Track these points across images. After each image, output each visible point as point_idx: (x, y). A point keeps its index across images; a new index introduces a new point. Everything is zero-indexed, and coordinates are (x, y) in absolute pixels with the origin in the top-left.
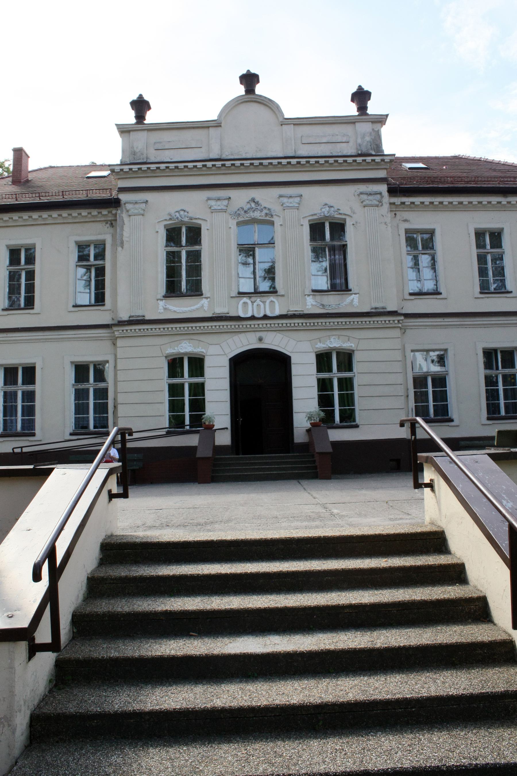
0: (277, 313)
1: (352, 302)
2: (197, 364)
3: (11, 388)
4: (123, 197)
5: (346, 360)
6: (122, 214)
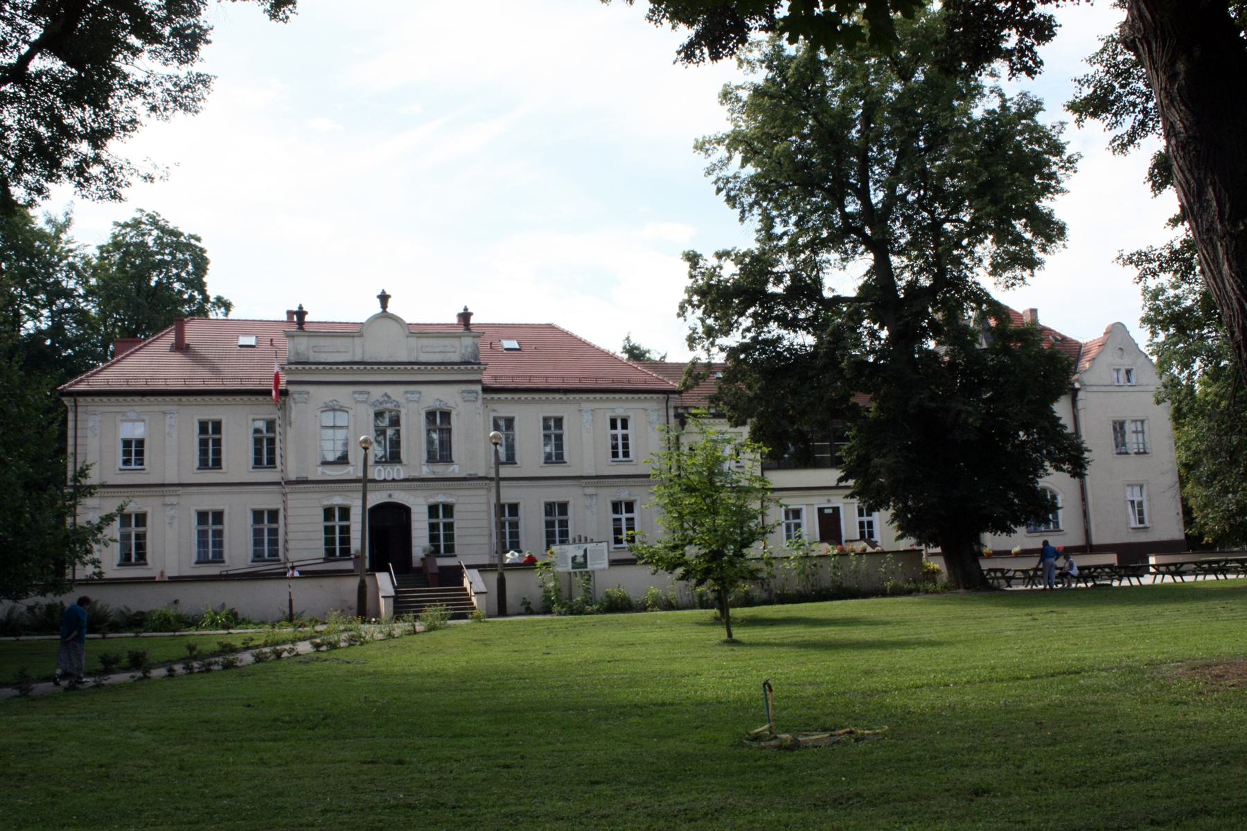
0: (402, 477)
1: (454, 470)
2: (345, 512)
3: (203, 527)
4: (291, 388)
5: (449, 509)
6: (290, 401)
